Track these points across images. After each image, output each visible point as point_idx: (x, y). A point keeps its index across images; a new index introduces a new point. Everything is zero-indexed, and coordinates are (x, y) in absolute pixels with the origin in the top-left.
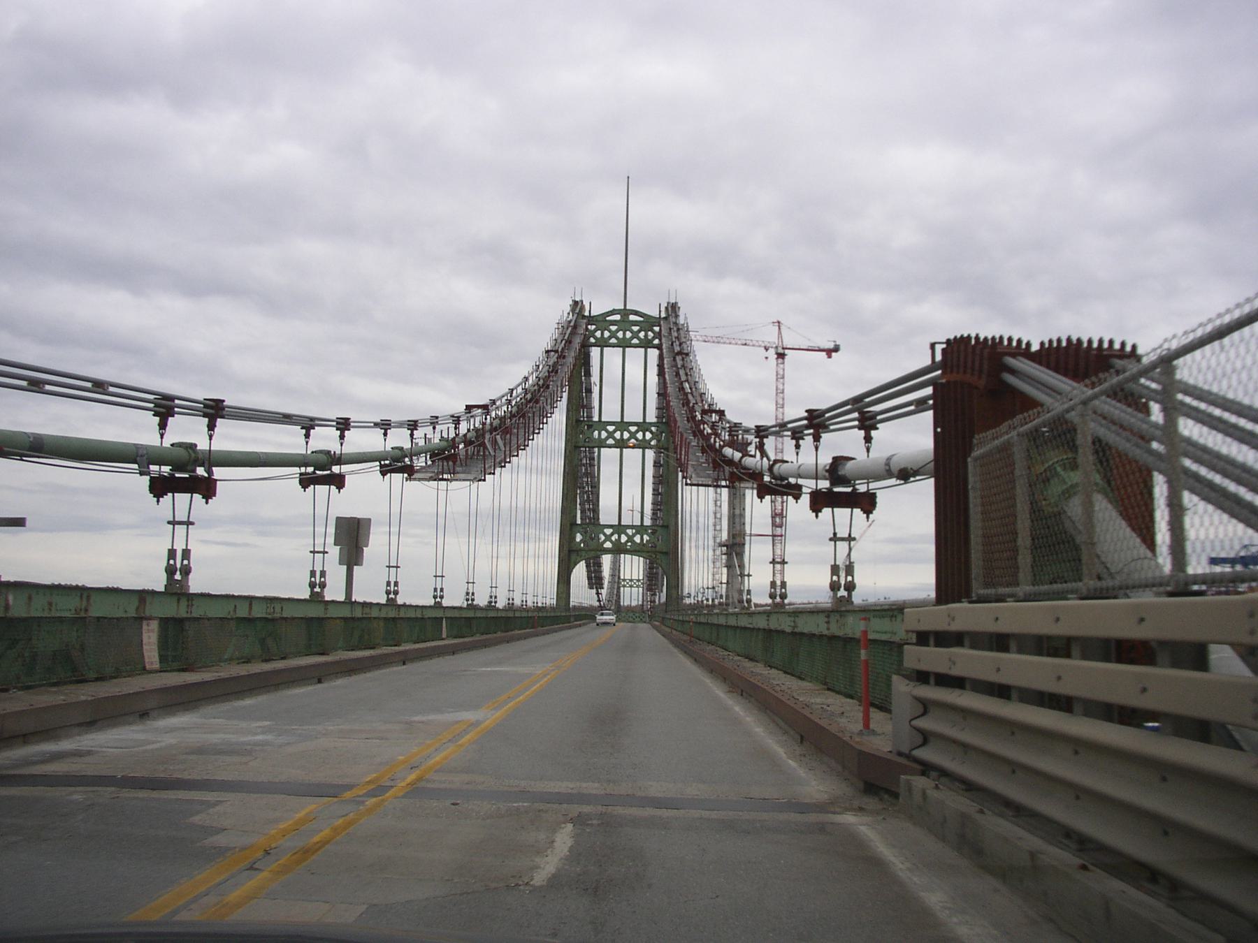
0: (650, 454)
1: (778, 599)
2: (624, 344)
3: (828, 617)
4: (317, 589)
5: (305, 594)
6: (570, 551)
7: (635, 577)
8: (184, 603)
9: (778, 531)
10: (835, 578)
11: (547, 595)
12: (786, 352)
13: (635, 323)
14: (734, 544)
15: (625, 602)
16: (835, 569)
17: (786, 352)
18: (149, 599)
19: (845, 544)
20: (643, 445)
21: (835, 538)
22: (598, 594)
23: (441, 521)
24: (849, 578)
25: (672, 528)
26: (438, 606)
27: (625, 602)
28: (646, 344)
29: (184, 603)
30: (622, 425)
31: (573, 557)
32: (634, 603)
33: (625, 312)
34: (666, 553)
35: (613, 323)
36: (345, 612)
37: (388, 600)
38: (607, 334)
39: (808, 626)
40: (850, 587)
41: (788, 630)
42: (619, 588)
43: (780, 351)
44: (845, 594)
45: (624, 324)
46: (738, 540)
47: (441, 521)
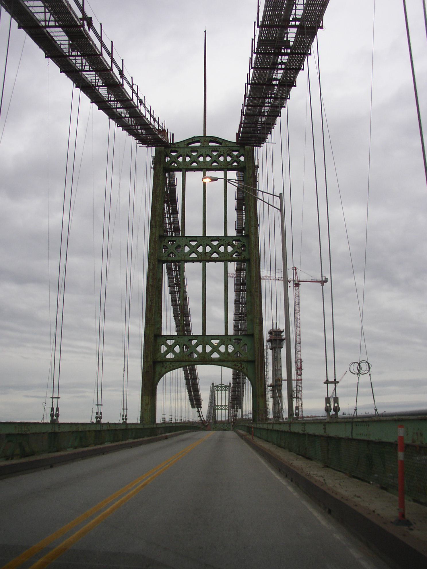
0: (232, 267)
1: (332, 413)
2: (204, 168)
3: (324, 425)
4: (55, 418)
5: (48, 420)
6: (155, 363)
7: (224, 404)
8: (57, 426)
9: (300, 377)
10: (328, 405)
11: (122, 405)
12: (300, 283)
13: (214, 149)
14: (276, 385)
15: (219, 419)
16: (328, 400)
17: (300, 283)
18: (291, 425)
19: (333, 385)
20: (225, 259)
21: (327, 382)
22: (198, 411)
23: (125, 383)
24: (336, 405)
25: (257, 336)
26: (124, 423)
27: (219, 419)
28: (225, 390)
29: (57, 426)
30: (204, 240)
31: (158, 368)
32: (224, 419)
33: (221, 385)
34: (252, 362)
35: (195, 149)
36: (123, 427)
37: (97, 421)
38: (200, 249)
39: (311, 430)
40: (337, 409)
41: (301, 432)
42: (215, 410)
43: (297, 282)
44: (334, 413)
45: (221, 387)
46: (279, 383)
47: (125, 383)
